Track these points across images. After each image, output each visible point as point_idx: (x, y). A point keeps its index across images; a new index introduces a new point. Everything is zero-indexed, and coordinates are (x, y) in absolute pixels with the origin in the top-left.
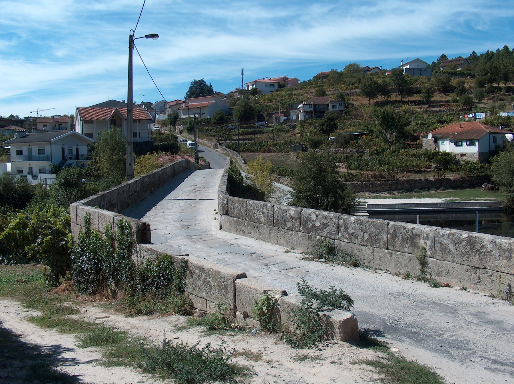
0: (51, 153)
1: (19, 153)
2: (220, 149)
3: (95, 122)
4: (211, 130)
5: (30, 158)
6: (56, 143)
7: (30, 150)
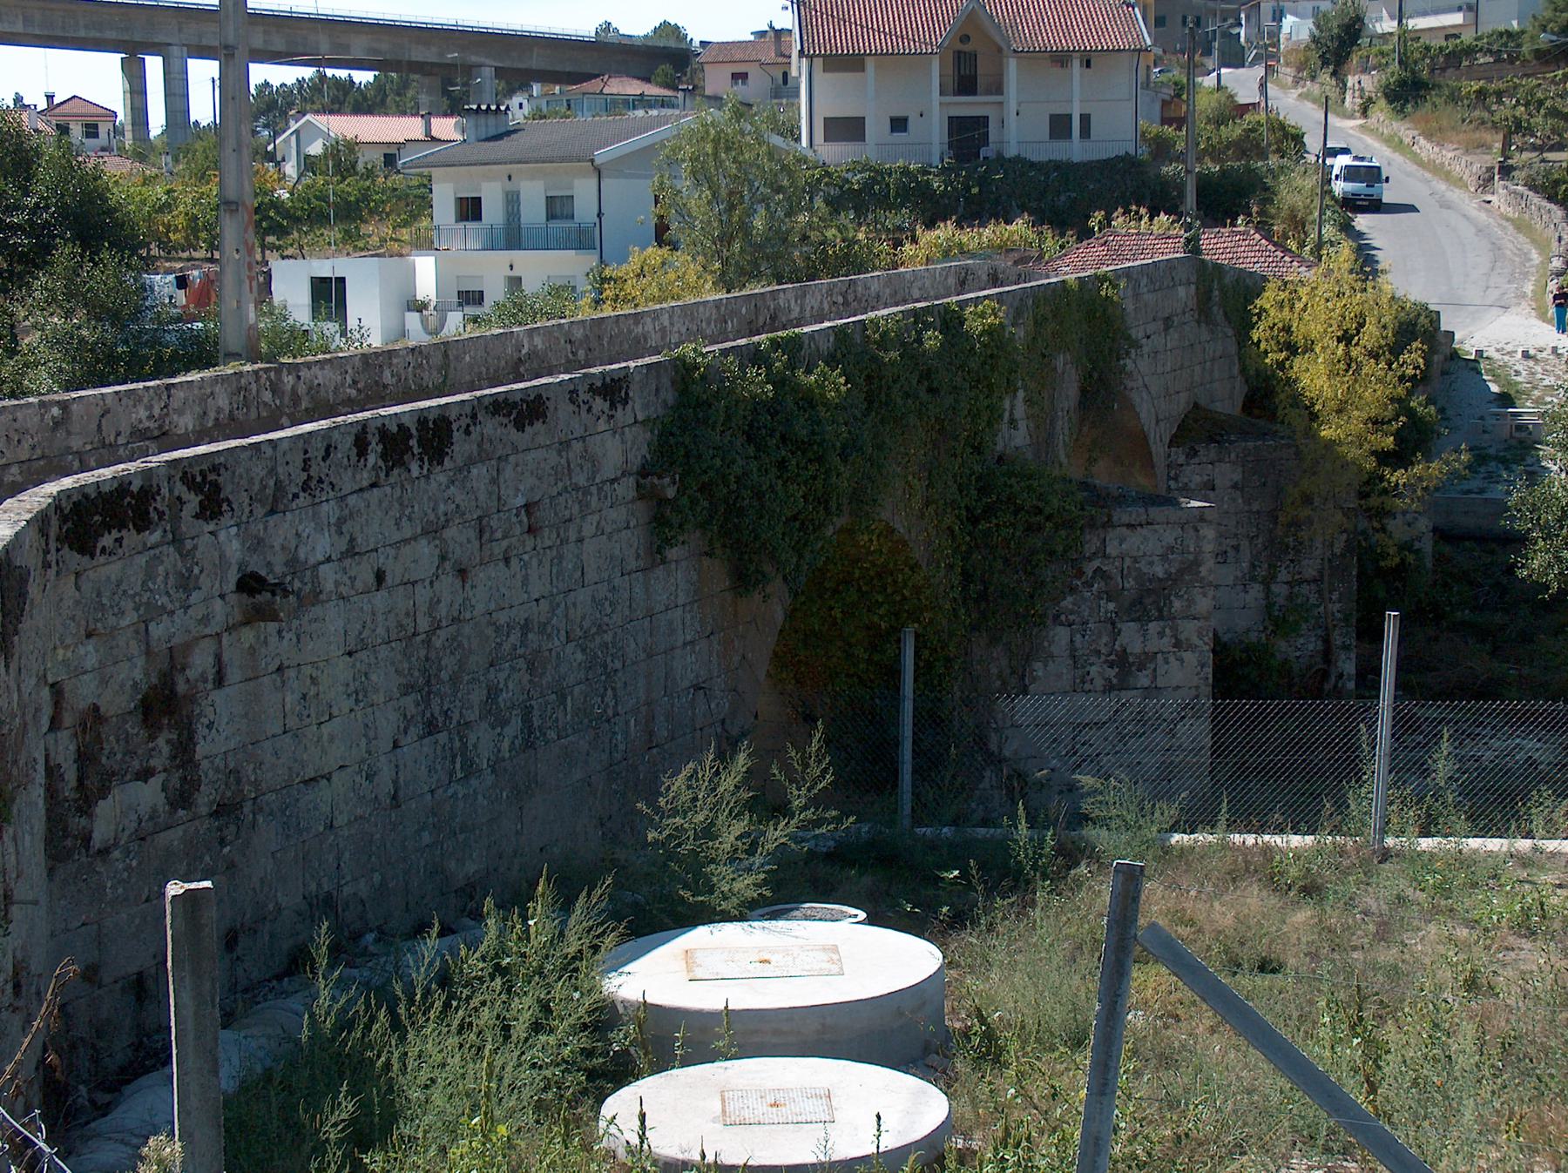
0: (600, 215)
1: (470, 209)
2: (1500, 196)
3: (870, 63)
4: (1499, 95)
5: (512, 237)
6: (622, 165)
7: (512, 201)
